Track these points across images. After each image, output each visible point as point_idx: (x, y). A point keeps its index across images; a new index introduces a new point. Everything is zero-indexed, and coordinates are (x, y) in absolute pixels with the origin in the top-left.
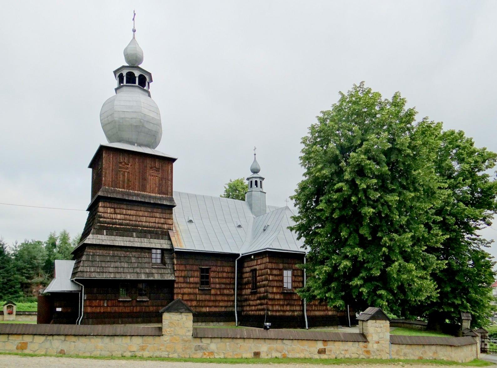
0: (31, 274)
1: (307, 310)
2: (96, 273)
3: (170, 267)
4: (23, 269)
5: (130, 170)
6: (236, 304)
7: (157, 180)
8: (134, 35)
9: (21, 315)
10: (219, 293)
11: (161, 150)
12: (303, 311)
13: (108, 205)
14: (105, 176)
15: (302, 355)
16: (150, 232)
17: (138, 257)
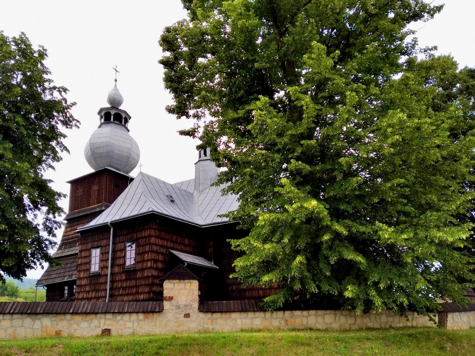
8: (116, 83)
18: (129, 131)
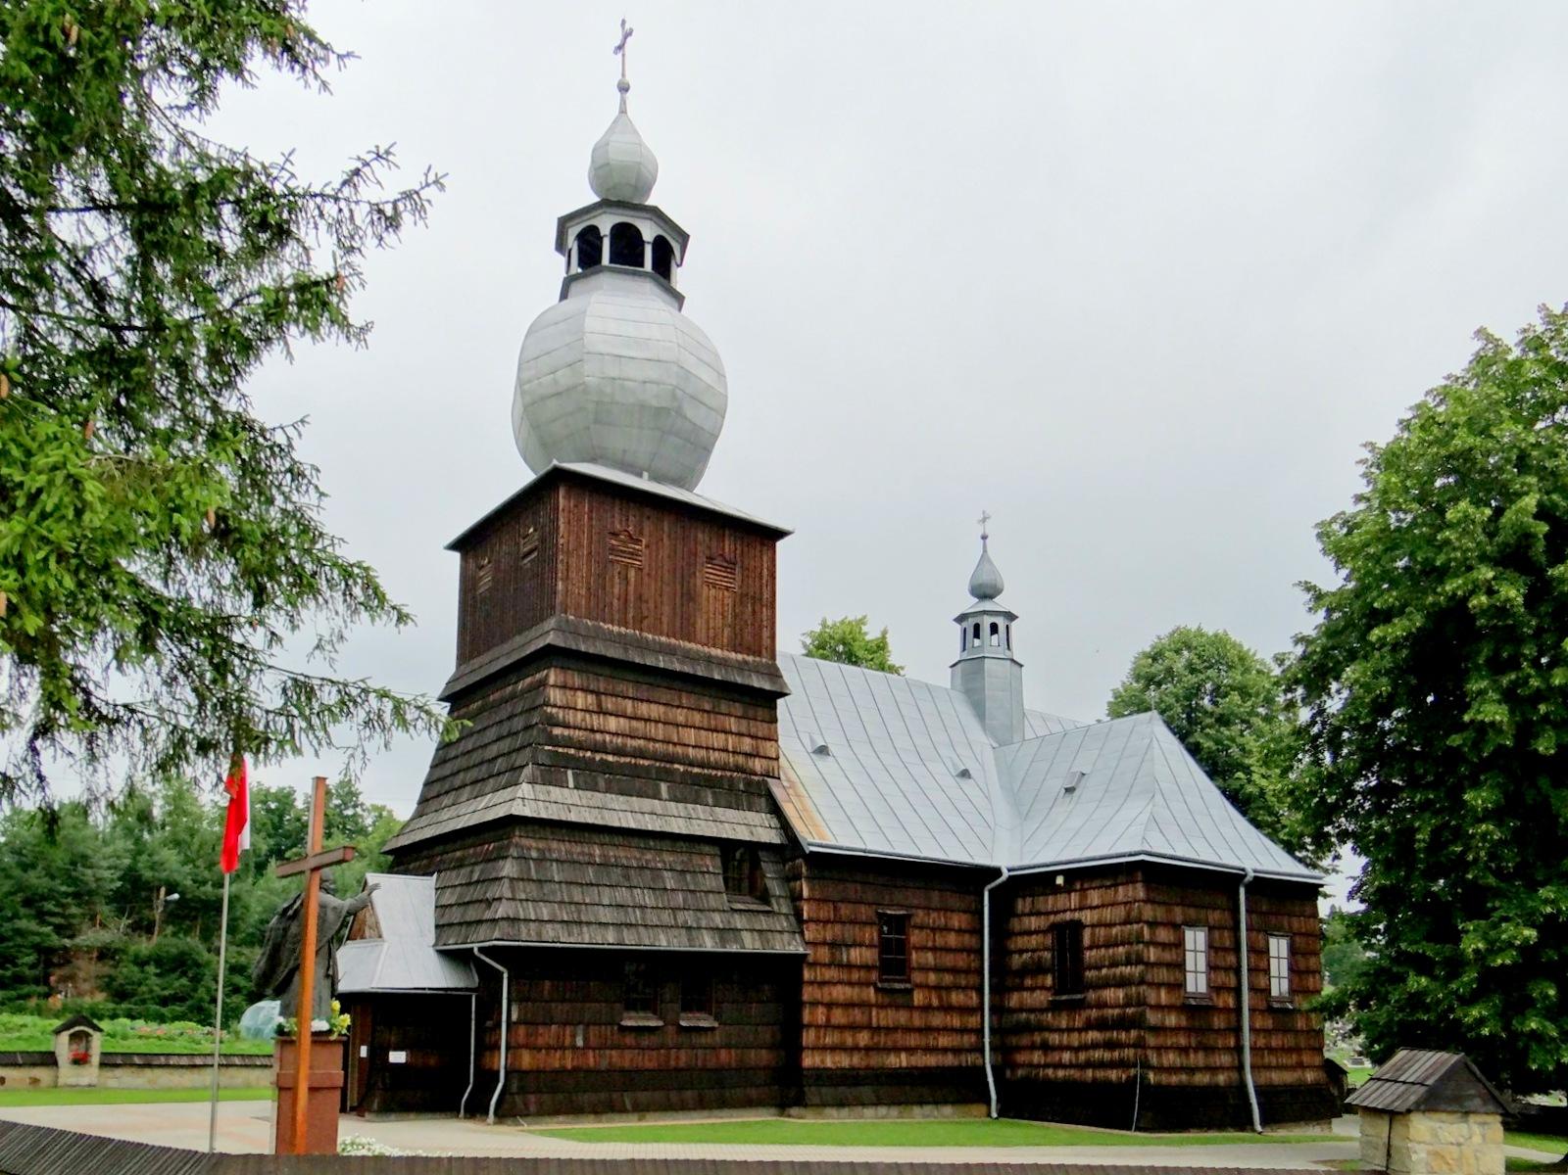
0: (73, 916)
1: (1252, 1067)
2: (558, 926)
3: (784, 910)
4: (44, 898)
5: (644, 561)
6: (987, 1040)
7: (729, 601)
8: (623, 102)
9: (117, 1066)
10: (935, 1002)
11: (713, 491)
12: (1240, 1068)
13: (576, 680)
14: (567, 578)
16: (710, 783)
17: (683, 872)
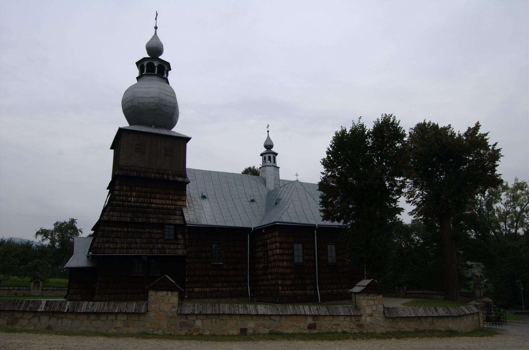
8: (156, 32)
15: (290, 331)
18: (168, 82)
